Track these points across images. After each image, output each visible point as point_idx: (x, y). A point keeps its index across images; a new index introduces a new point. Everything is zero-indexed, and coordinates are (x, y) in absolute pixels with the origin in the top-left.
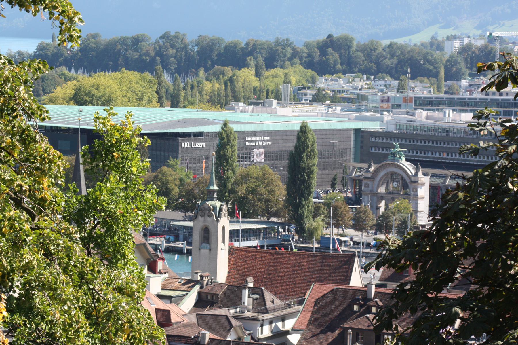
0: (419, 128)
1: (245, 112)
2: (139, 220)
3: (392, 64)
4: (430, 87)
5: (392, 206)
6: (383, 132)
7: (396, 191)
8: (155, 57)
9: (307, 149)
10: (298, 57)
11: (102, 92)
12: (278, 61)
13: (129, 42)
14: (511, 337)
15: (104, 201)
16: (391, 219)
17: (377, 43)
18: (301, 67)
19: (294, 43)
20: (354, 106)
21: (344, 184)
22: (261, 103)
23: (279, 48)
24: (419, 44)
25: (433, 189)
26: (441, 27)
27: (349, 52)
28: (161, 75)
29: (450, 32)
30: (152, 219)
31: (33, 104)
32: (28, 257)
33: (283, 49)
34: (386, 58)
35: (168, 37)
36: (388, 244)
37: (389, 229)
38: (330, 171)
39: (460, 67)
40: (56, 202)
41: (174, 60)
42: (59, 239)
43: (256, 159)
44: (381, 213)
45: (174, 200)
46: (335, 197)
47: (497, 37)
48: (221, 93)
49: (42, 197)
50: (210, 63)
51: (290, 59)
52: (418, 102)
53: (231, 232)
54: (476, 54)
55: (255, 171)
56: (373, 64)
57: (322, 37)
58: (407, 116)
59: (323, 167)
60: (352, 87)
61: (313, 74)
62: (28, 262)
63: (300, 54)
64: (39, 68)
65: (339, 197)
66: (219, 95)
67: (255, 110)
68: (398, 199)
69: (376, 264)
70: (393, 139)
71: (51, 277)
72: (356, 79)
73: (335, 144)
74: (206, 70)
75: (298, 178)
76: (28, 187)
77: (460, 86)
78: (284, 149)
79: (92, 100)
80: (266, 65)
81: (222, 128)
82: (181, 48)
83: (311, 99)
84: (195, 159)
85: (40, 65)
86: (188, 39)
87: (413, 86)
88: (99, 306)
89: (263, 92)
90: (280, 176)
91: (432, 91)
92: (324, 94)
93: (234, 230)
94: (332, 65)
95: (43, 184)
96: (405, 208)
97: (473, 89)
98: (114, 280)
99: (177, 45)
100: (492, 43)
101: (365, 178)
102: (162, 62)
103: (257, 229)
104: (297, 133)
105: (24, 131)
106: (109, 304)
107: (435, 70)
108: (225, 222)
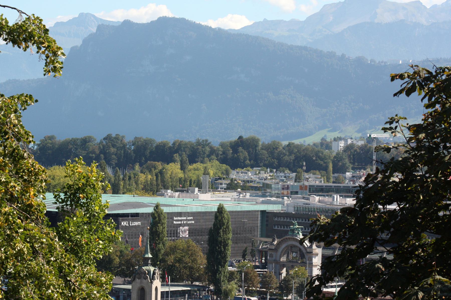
0: (312, 209)
1: (172, 197)
2: (100, 248)
3: (291, 160)
4: (321, 178)
5: (292, 272)
6: (284, 213)
7: (295, 260)
8: (99, 155)
9: (223, 226)
10: (214, 154)
11: (57, 182)
12: (199, 158)
13: (79, 142)
14: (425, 283)
15: (72, 232)
16: (291, 282)
17: (279, 143)
18: (217, 162)
19: (212, 143)
20: (260, 193)
21: (253, 255)
22: (185, 190)
23: (200, 147)
24: (311, 144)
25: (324, 258)
26: (329, 131)
27: (256, 150)
28: (105, 168)
29: (336, 134)
30: (110, 248)
31: (21, 130)
32: (19, 246)
33: (202, 147)
34: (286, 155)
35: (110, 138)
36: (319, 221)
37: (290, 291)
38: (242, 245)
39: (345, 162)
40: (39, 210)
41: (115, 157)
42: (42, 238)
43: (181, 235)
44: (283, 278)
45: (115, 268)
46: (246, 265)
47: (374, 138)
48: (153, 182)
49: (29, 204)
50: (144, 159)
51: (209, 156)
52: (312, 189)
53: (162, 293)
54: (357, 152)
55: (181, 244)
56: (275, 160)
57: (234, 138)
58: (303, 200)
59: (236, 241)
60: (259, 178)
61: (227, 168)
62: (20, 250)
63: (217, 152)
64: (26, 102)
65: (249, 265)
66: (151, 184)
67: (180, 196)
68: (297, 266)
69: (309, 238)
70: (292, 219)
71: (37, 267)
72: (261, 172)
73: (245, 223)
74: (141, 165)
75: (216, 249)
76: (20, 188)
77: (345, 178)
78: (204, 227)
79: (49, 188)
80: (189, 161)
81: (154, 209)
82: (120, 147)
83: (225, 187)
84: (132, 235)
85: (27, 98)
86: (126, 140)
87: (307, 177)
88: (74, 295)
89: (187, 182)
90: (201, 248)
91: (323, 182)
92: (236, 184)
93: (164, 292)
94: (242, 161)
95: (30, 193)
96: (302, 274)
97: (355, 179)
98: (86, 274)
99: (118, 144)
100: (370, 144)
101: (270, 249)
102: (105, 159)
103: (182, 290)
104: (215, 214)
105: (14, 150)
106: (83, 292)
107: (325, 165)
108: (157, 283)
